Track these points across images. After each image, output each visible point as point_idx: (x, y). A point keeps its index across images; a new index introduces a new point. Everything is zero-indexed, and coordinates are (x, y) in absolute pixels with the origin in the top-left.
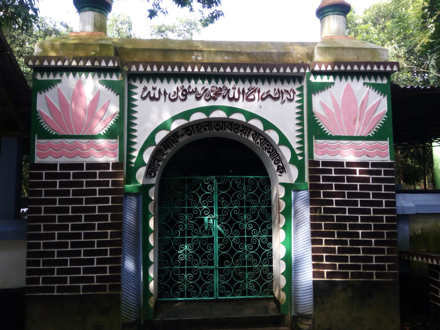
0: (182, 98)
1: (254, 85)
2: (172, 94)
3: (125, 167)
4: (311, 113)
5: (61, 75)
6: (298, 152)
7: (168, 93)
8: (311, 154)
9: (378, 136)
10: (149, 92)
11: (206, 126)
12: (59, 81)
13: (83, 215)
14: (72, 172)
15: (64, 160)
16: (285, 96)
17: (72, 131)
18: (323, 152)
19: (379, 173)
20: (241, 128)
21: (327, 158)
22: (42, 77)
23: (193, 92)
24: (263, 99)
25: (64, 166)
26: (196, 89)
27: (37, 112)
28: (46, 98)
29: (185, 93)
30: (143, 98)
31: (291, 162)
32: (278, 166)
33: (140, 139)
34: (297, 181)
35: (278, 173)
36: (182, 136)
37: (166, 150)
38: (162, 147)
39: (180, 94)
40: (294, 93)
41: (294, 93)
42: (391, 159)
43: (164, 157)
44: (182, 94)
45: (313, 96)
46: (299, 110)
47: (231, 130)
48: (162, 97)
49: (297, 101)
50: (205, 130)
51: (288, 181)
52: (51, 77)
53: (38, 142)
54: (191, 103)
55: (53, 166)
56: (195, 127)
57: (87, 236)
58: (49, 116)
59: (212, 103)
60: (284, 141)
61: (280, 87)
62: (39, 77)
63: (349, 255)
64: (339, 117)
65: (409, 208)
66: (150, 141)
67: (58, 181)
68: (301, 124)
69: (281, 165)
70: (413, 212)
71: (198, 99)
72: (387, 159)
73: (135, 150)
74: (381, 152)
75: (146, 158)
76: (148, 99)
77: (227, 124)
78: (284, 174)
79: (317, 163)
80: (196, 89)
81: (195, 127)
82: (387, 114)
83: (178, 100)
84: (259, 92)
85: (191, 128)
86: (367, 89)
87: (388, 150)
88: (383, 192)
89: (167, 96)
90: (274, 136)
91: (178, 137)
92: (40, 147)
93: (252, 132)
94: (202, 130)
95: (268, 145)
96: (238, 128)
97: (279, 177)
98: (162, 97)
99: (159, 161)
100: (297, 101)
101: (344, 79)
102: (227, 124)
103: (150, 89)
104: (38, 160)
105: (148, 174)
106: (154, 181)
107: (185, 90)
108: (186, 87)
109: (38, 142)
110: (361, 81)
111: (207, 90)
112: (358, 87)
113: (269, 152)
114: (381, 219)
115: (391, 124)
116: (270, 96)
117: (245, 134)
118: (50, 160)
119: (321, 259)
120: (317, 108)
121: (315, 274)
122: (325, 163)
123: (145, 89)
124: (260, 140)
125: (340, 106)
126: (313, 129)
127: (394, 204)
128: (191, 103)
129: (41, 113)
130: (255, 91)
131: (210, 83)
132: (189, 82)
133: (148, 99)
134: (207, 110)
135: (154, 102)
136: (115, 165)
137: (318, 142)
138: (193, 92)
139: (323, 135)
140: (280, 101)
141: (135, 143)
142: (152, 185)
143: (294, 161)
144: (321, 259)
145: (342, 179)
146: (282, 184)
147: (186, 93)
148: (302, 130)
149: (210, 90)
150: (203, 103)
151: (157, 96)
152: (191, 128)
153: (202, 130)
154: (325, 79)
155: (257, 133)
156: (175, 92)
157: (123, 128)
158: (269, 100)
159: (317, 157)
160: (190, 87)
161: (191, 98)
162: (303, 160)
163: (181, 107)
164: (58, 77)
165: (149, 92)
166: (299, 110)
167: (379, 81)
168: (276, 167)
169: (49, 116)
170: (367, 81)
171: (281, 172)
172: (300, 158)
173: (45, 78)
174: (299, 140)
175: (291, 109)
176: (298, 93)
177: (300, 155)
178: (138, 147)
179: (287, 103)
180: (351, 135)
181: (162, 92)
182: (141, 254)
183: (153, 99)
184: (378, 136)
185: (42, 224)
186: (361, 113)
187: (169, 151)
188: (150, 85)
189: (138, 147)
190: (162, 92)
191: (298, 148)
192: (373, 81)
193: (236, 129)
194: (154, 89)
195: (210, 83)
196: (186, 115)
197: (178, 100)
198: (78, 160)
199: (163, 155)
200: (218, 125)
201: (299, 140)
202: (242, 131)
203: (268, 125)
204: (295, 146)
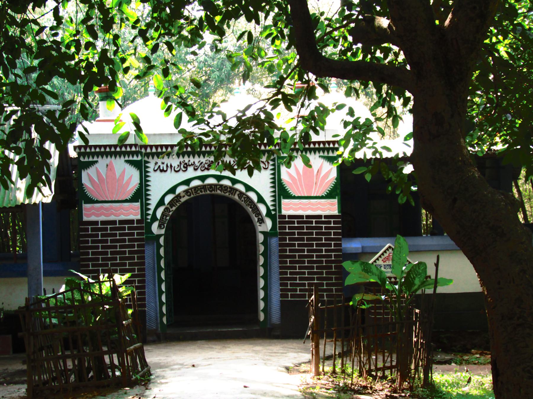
0: (184, 169)
2: (176, 167)
3: (144, 223)
4: (280, 180)
5: (98, 157)
6: (271, 208)
7: (173, 165)
8: (280, 211)
9: (329, 195)
10: (159, 166)
11: (202, 188)
12: (97, 162)
13: (90, 263)
14: (109, 227)
15: (123, 217)
17: (107, 197)
18: (289, 208)
20: (229, 190)
22: (84, 159)
23: (192, 165)
25: (103, 223)
26: (194, 162)
27: (83, 185)
28: (88, 174)
29: (185, 166)
30: (155, 171)
32: (258, 219)
33: (153, 202)
34: (270, 230)
35: (258, 224)
36: (184, 196)
37: (172, 208)
39: (182, 167)
41: (268, 163)
42: (339, 212)
44: (184, 167)
47: (221, 191)
48: (169, 169)
49: (272, 170)
50: (201, 192)
51: (266, 230)
52: (91, 159)
53: (86, 206)
54: (191, 173)
55: (96, 223)
56: (193, 190)
58: (92, 188)
59: (206, 173)
60: (261, 200)
62: (82, 159)
63: (306, 282)
65: (357, 248)
66: (161, 202)
67: (100, 233)
68: (274, 187)
69: (260, 217)
70: (360, 251)
71: (196, 170)
72: (336, 212)
73: (149, 209)
74: (331, 208)
76: (159, 170)
77: (218, 187)
78: (263, 225)
79: (284, 217)
80: (194, 162)
81: (193, 190)
82: (336, 179)
83: (181, 171)
85: (190, 191)
86: (321, 160)
87: (337, 206)
88: (332, 236)
89: (173, 169)
90: (252, 196)
91: (181, 197)
92: (87, 209)
93: (238, 193)
94: (199, 192)
95: (250, 202)
96: (226, 190)
97: (259, 227)
98: (169, 169)
99: (167, 216)
100: (272, 170)
102: (218, 187)
103: (160, 164)
104: (85, 219)
107: (186, 164)
108: (187, 161)
109: (86, 206)
110: (317, 154)
111: (202, 163)
112: (119, 164)
113: (251, 208)
114: (330, 256)
115: (339, 187)
117: (232, 194)
118: (93, 218)
121: (282, 296)
122: (290, 217)
123: (156, 163)
124: (244, 198)
125: (301, 174)
126: (281, 191)
127: (340, 245)
128: (191, 173)
129: (86, 185)
131: (204, 157)
132: (189, 157)
133: (159, 170)
134: (203, 178)
135: (163, 173)
136: (138, 221)
137: (284, 201)
138: (192, 165)
139: (289, 196)
143: (269, 214)
145: (303, 228)
146: (261, 232)
147: (186, 166)
148: (274, 192)
149: (204, 162)
150: (199, 173)
151: (165, 169)
152: (190, 191)
153: (199, 192)
155: (241, 194)
156: (178, 165)
157: (141, 195)
159: (284, 212)
160: (189, 161)
161: (191, 169)
162: (276, 214)
163: (183, 176)
164: (95, 159)
165: (159, 166)
167: (135, 158)
168: (256, 219)
169: (92, 188)
171: (260, 223)
172: (273, 213)
173: (86, 159)
174: (273, 199)
177: (273, 210)
178: (152, 207)
180: (309, 195)
181: (169, 165)
182: (157, 285)
183: (162, 171)
184: (329, 195)
185: (90, 263)
186: (316, 179)
187: (174, 208)
188: (160, 161)
189: (152, 207)
190: (169, 165)
191: (272, 205)
192: (326, 154)
193: (225, 190)
194: (163, 163)
195: (204, 157)
196: (187, 182)
197: (181, 171)
198: (112, 218)
199: (170, 211)
201: (273, 199)
202: (229, 192)
204: (269, 203)
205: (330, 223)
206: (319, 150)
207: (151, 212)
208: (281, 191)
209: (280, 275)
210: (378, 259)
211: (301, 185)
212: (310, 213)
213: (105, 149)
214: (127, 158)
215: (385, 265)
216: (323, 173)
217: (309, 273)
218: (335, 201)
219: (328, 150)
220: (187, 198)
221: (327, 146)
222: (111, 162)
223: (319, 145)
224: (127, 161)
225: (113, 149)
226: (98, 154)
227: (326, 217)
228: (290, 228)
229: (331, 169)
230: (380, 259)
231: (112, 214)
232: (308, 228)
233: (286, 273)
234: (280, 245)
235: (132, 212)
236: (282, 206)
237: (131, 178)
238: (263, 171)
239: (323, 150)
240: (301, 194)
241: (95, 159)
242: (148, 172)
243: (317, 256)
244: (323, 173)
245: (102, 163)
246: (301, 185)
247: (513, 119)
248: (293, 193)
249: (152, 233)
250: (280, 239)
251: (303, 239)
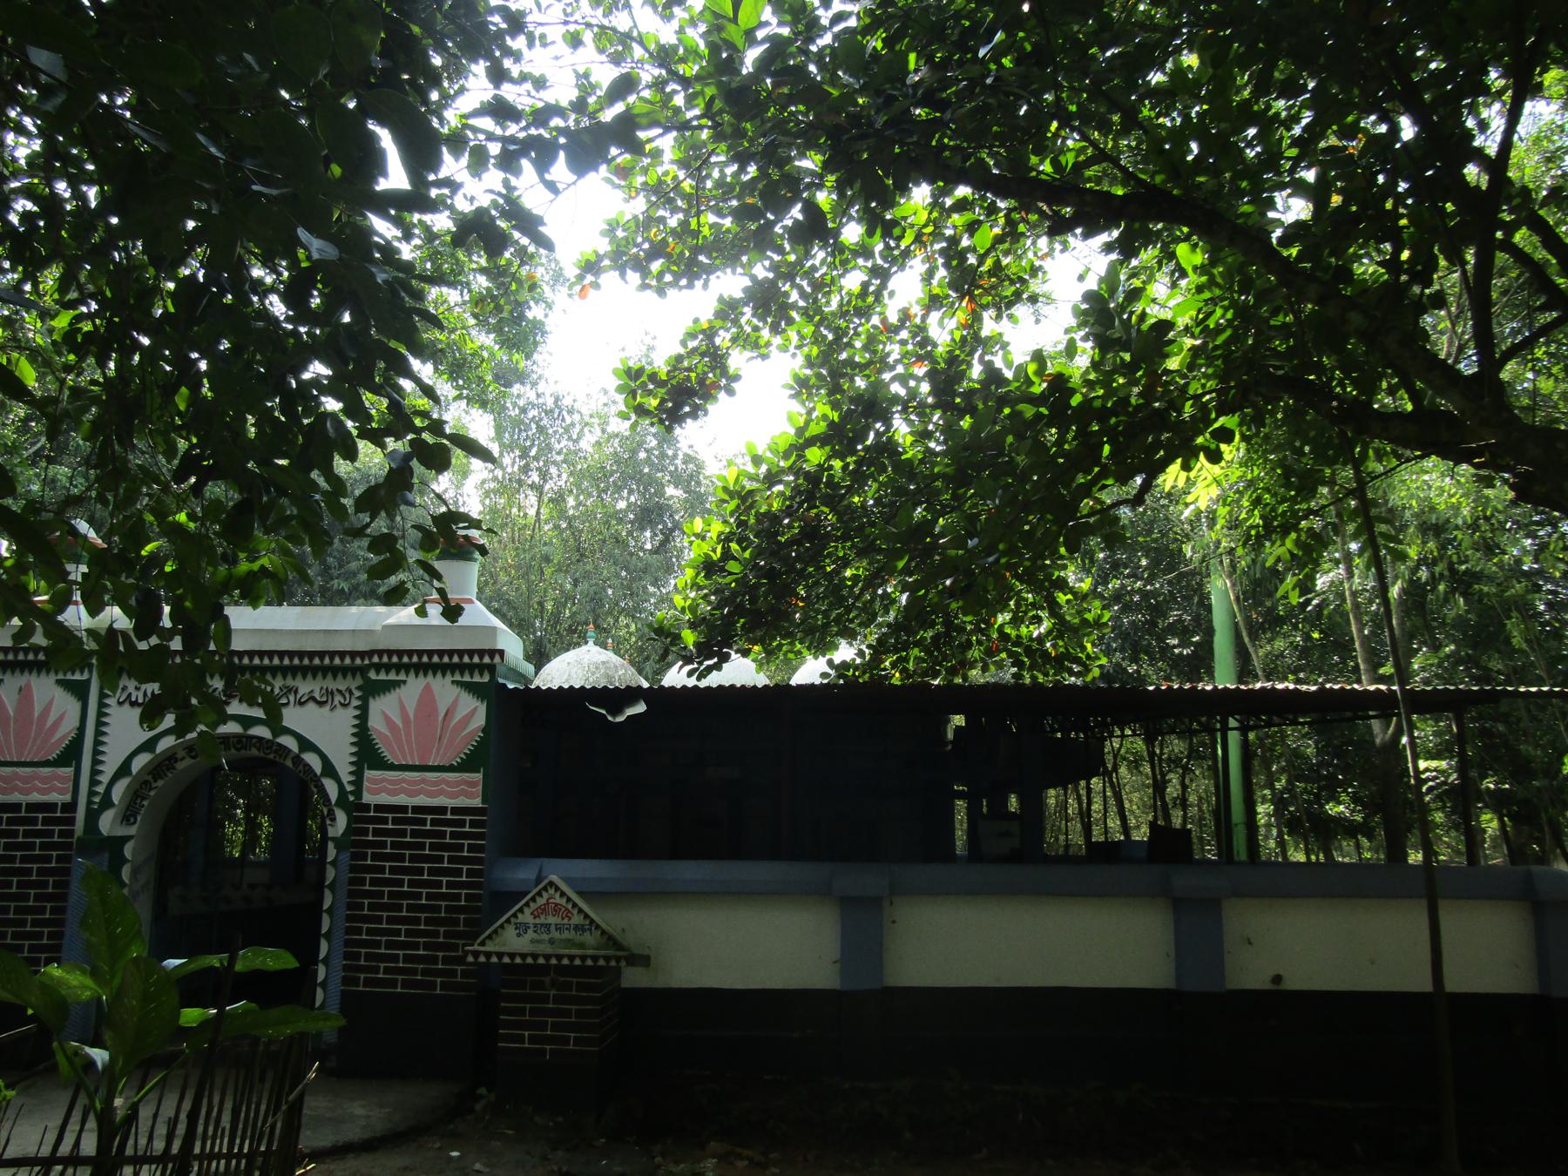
1: (290, 682)
6: (349, 788)
15: (36, 797)
16: (338, 698)
18: (381, 790)
19: (462, 823)
21: (384, 799)
24: (301, 704)
25: (33, 807)
30: (120, 704)
31: (338, 803)
38: (150, 778)
40: (351, 693)
43: (152, 793)
45: (371, 701)
46: (101, 758)
49: (356, 708)
52: (392, 676)
57: (18, 910)
60: (329, 770)
61: (330, 684)
64: (408, 735)
66: (124, 770)
72: (477, 802)
73: (100, 782)
75: (117, 793)
76: (127, 705)
79: (367, 807)
84: (296, 692)
86: (456, 690)
99: (143, 799)
101: (421, 674)
105: (127, 817)
106: (133, 830)
110: (449, 678)
112: (445, 690)
116: (313, 699)
119: (357, 956)
120: (375, 723)
122: (379, 808)
126: (367, 753)
130: (290, 691)
133: (127, 705)
137: (369, 774)
139: (381, 764)
140: (328, 707)
141: (101, 772)
142: (129, 838)
144: (357, 956)
154: (392, 676)
158: (311, 706)
159: (367, 798)
164: (402, 677)
166: (101, 758)
167: (477, 679)
170: (458, 677)
173: (382, 676)
175: (345, 719)
176: (357, 693)
178: (105, 779)
179: (340, 710)
184: (466, 765)
187: (160, 783)
189: (105, 779)
192: (467, 678)
198: (16, 797)
200: (240, 741)
203: (306, 745)
204: (346, 778)
205: (462, 823)
206: (452, 668)
207: (100, 789)
208: (367, 753)
209: (347, 933)
210: (521, 910)
211: (409, 742)
212: (423, 800)
213: (461, 658)
214: (61, 676)
215: (535, 925)
216: (458, 716)
217: (447, 935)
218: (478, 777)
219: (471, 668)
220: (188, 762)
221: (466, 659)
222: (28, 686)
223: (481, 658)
224: (59, 682)
225: (415, 659)
226: (407, 668)
227: (455, 810)
228: (376, 832)
229: (476, 709)
230: (527, 910)
231: (15, 789)
232: (414, 834)
233: (359, 931)
234: (353, 869)
235: (52, 788)
236: (365, 783)
237: (61, 717)
238: (340, 711)
239: (462, 668)
240: (405, 758)
241: (402, 677)
242: (107, 706)
243: (429, 897)
244: (458, 716)
245: (414, 687)
246: (409, 742)
247: (77, 597)
248: (390, 758)
249: (100, 833)
250: (354, 856)
251: (401, 858)
